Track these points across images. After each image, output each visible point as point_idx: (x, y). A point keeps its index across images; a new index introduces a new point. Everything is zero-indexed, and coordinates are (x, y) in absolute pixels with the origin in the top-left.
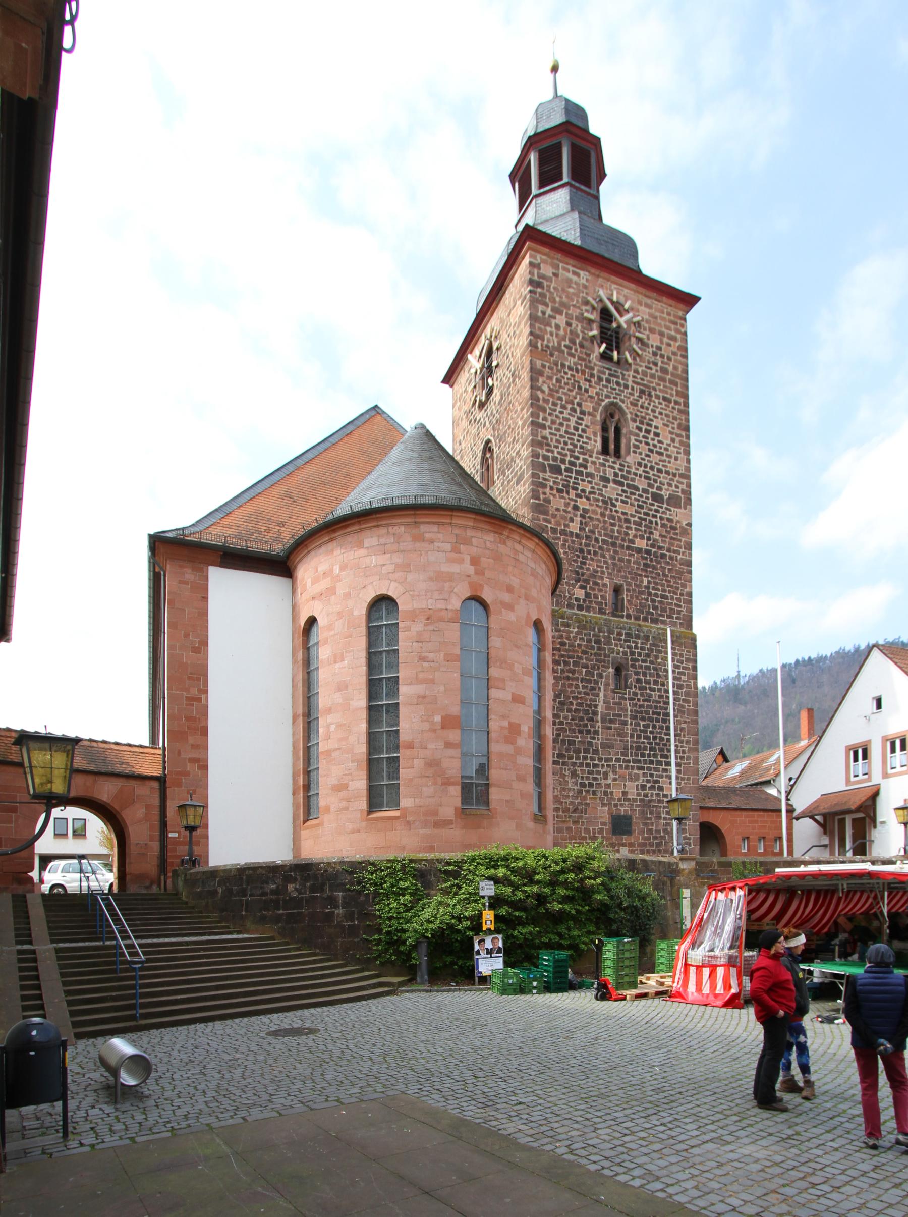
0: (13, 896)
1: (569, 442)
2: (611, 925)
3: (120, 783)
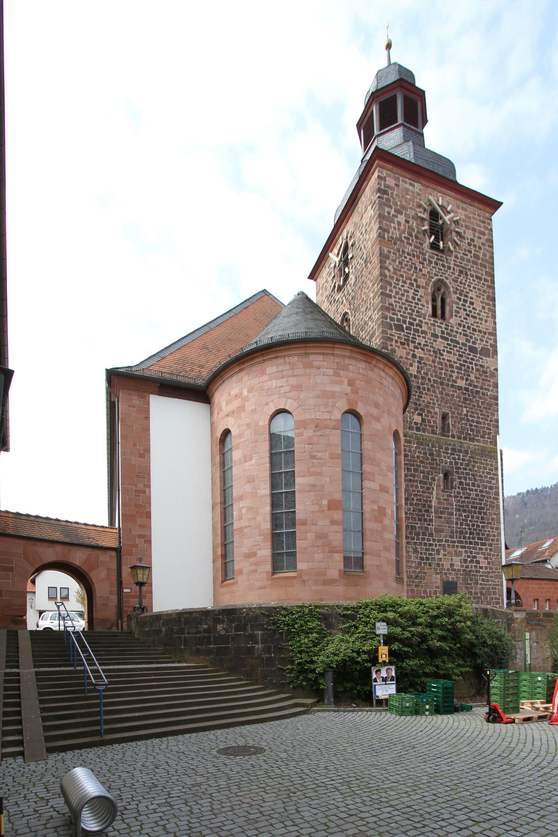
0: (8, 631)
2: (476, 660)
3: (88, 552)
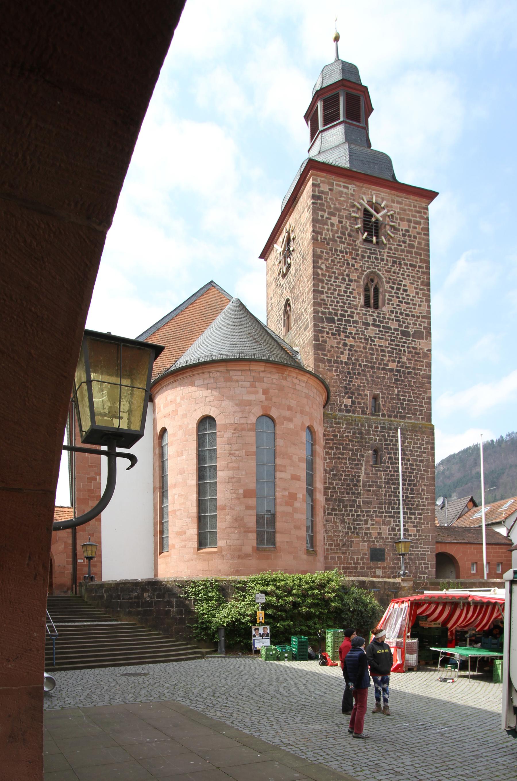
1: (340, 301)
